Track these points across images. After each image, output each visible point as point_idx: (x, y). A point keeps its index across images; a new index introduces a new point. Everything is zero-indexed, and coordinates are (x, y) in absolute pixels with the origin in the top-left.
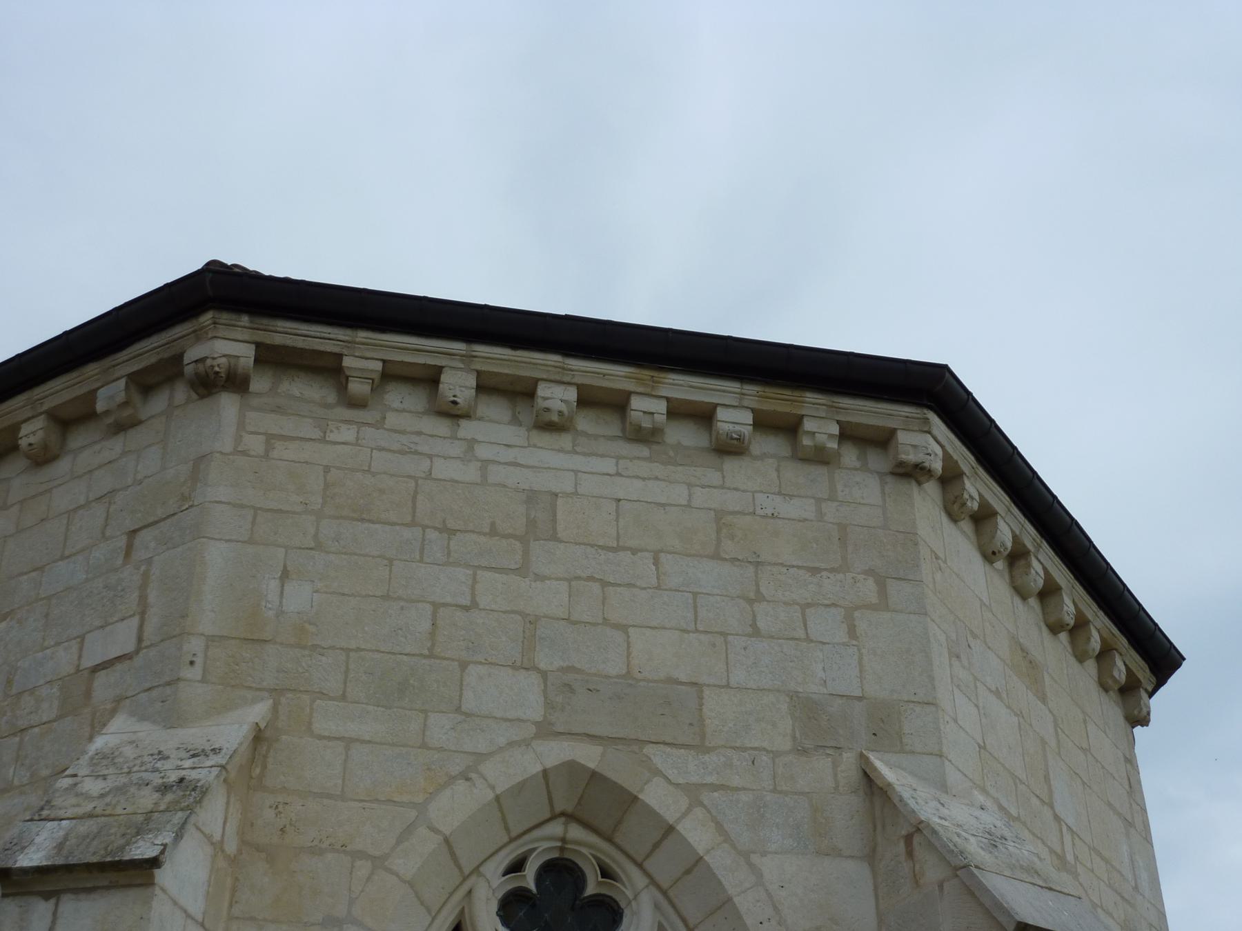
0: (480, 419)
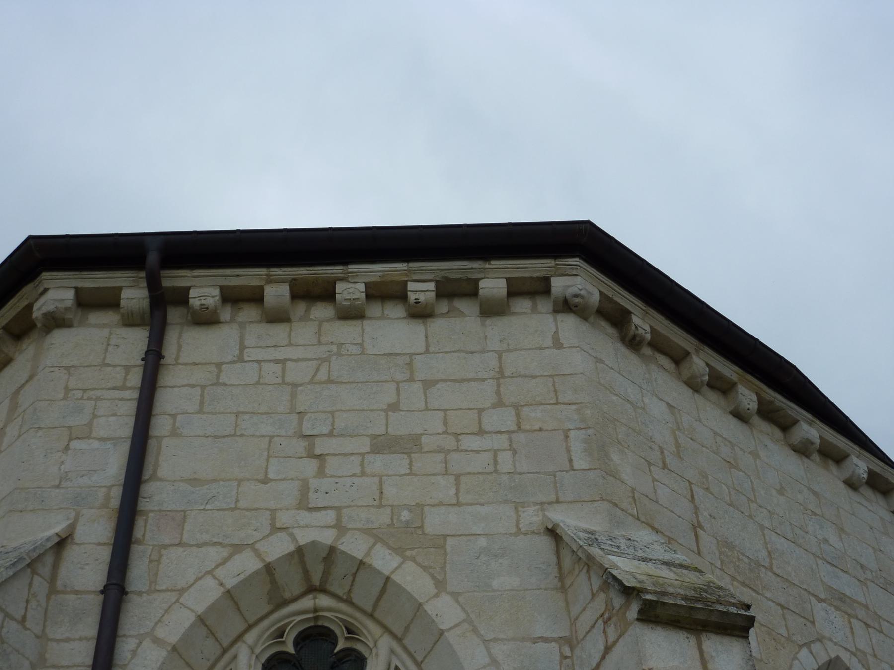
0: (370, 318)
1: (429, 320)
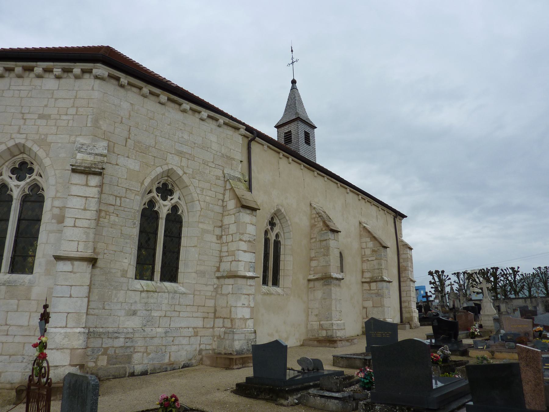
1: (61, 79)
